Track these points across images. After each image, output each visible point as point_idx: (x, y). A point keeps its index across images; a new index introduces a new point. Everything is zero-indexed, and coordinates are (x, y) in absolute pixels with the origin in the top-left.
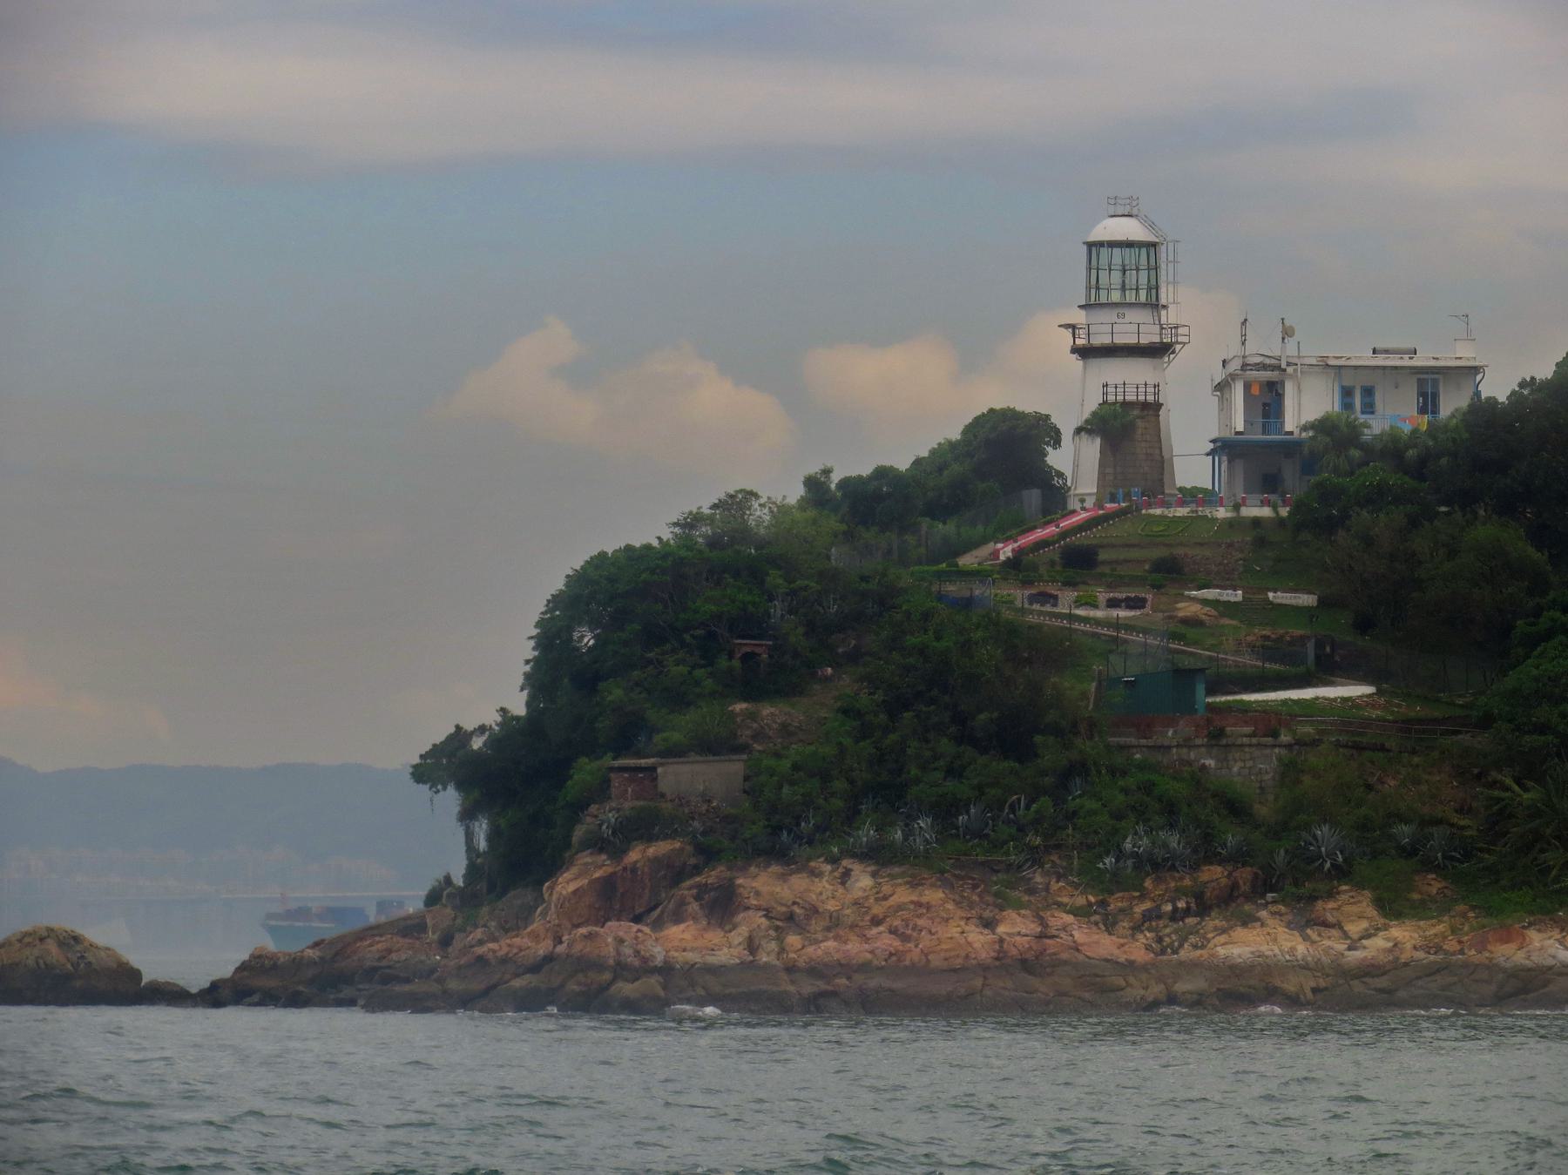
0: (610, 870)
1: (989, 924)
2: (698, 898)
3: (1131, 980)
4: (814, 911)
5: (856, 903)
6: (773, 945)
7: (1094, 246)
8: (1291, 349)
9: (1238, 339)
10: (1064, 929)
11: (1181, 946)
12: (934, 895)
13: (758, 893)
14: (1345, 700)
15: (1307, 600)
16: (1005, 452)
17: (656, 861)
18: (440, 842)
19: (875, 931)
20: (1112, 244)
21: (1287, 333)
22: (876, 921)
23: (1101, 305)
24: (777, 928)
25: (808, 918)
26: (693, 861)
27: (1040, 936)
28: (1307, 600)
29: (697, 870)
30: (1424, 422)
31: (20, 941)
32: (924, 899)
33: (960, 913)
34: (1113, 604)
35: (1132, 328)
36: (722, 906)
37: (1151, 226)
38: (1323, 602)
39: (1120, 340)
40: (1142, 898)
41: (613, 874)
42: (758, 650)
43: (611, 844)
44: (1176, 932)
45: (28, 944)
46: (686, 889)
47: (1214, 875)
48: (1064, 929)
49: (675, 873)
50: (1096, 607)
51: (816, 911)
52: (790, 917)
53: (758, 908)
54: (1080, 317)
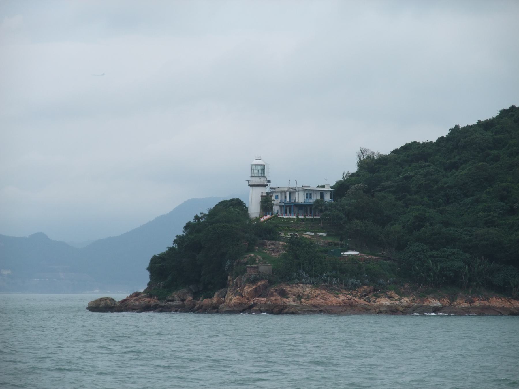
2: (276, 292)
7: (252, 165)
12: (324, 292)
13: (290, 291)
17: (263, 285)
18: (141, 282)
20: (256, 165)
22: (317, 297)
28: (325, 235)
35: (262, 181)
43: (254, 281)
52: (299, 296)
54: (250, 179)
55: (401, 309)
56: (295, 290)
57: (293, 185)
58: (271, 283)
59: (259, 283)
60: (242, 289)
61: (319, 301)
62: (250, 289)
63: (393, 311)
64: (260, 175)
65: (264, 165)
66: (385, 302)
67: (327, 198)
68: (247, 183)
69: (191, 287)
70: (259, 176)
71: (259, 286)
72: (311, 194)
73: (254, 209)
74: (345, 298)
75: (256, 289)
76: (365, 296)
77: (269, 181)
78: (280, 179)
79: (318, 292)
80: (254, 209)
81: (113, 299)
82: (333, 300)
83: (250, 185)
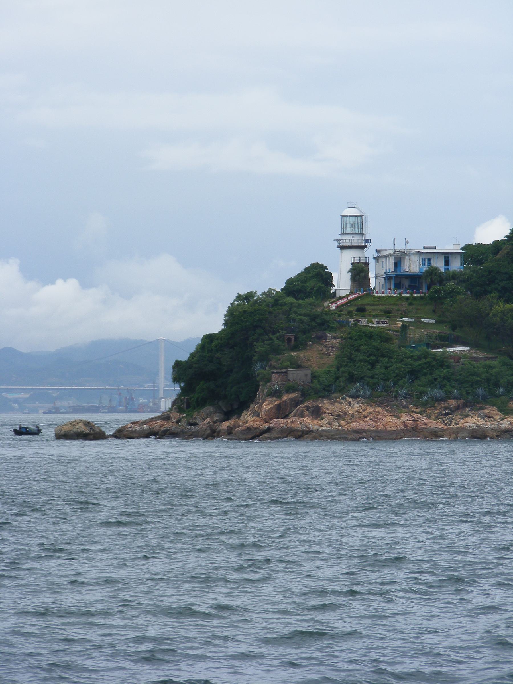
0: (279, 402)
1: (399, 417)
2: (307, 410)
3: (445, 433)
4: (346, 414)
5: (357, 411)
6: (337, 424)
7: (343, 216)
8: (408, 248)
9: (393, 244)
10: (419, 418)
11: (451, 423)
12: (379, 409)
13: (328, 409)
14: (464, 351)
15: (432, 321)
16: (317, 278)
17: (292, 400)
18: (165, 393)
19: (366, 420)
20: (350, 216)
21: (407, 242)
22: (366, 417)
23: (347, 234)
24: (336, 419)
25: (345, 416)
26: (301, 399)
27: (414, 421)
28: (432, 321)
29: (302, 402)
30: (425, 268)
31: (71, 424)
32: (377, 410)
33: (389, 414)
34: (378, 323)
35: (355, 240)
36: (317, 413)
37: (361, 211)
38: (436, 322)
39: (346, 245)
40: (436, 409)
41: (280, 403)
42: (291, 337)
43: (276, 394)
44: (448, 419)
45: (74, 425)
46: (301, 407)
47: (453, 403)
48: (419, 418)
49: (296, 403)
50: (373, 324)
51: (347, 414)
52: (339, 415)
53: (329, 413)
54: (340, 237)
55: (491, 433)
56: (336, 407)
57: (400, 246)
58: (305, 395)
59: (285, 398)
60: (260, 407)
61: (367, 424)
62: (269, 407)
63: (479, 436)
64: (356, 231)
65: (361, 216)
66: (473, 422)
67: (456, 265)
68: (336, 244)
69: (220, 403)
70: (354, 234)
71: (285, 402)
72: (429, 260)
73: (342, 283)
74: (410, 418)
75: (279, 406)
76: (446, 414)
77: (367, 241)
78: (385, 236)
79: (369, 409)
80: (342, 283)
81: (89, 423)
82: (392, 422)
83: (338, 247)
